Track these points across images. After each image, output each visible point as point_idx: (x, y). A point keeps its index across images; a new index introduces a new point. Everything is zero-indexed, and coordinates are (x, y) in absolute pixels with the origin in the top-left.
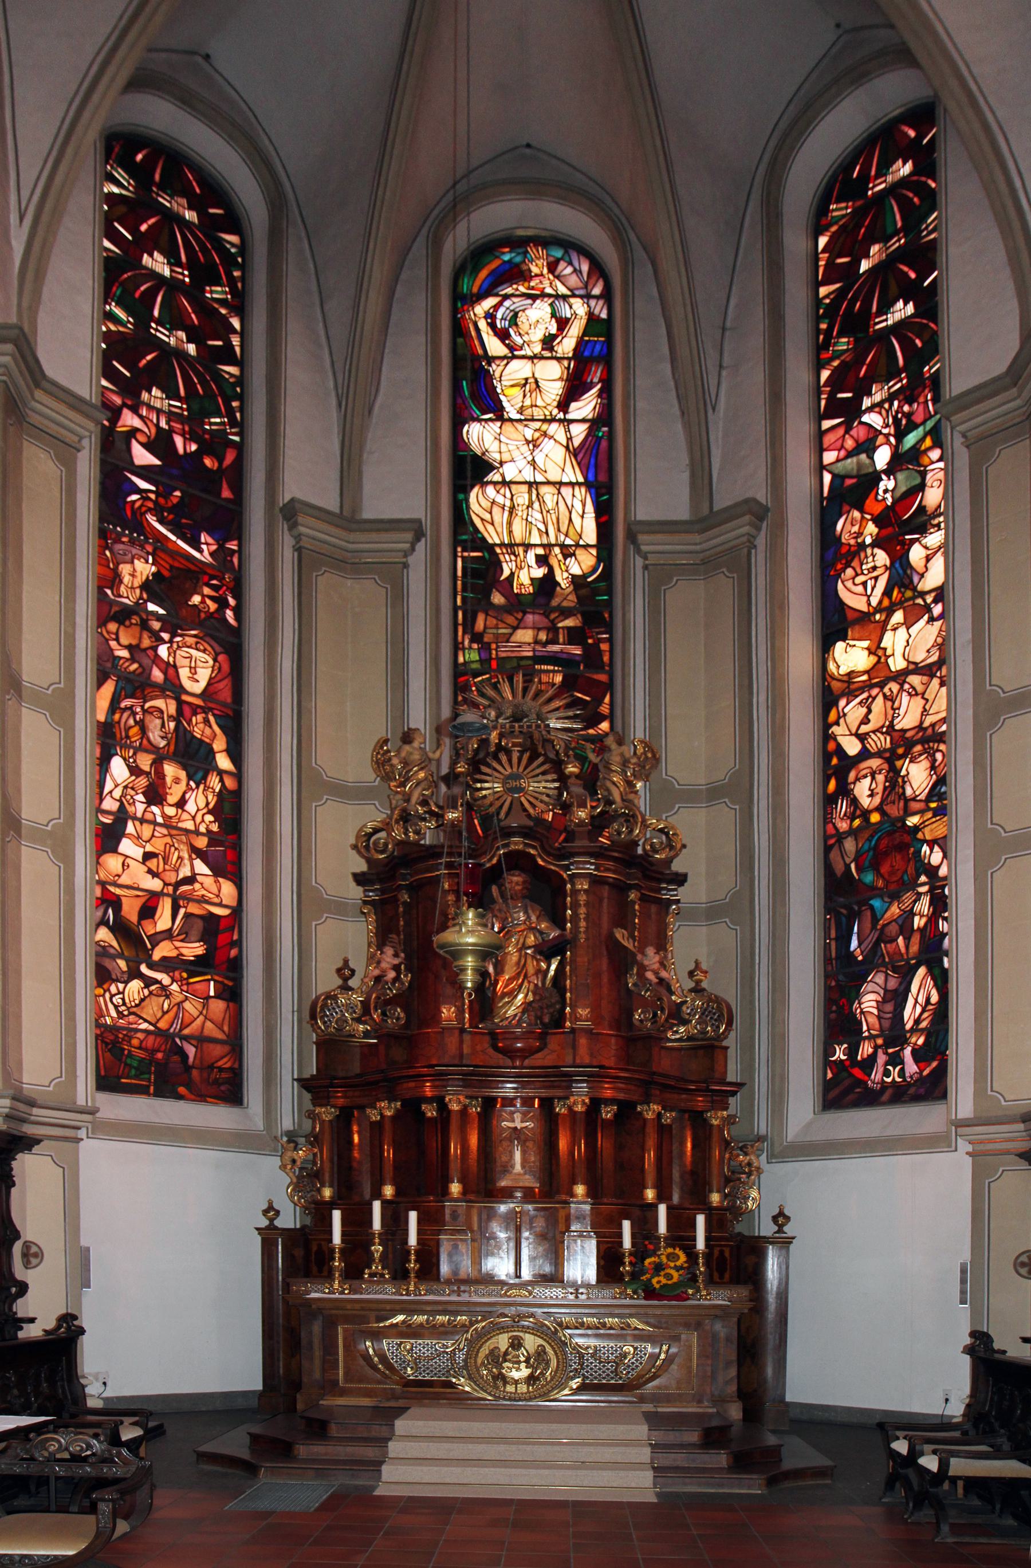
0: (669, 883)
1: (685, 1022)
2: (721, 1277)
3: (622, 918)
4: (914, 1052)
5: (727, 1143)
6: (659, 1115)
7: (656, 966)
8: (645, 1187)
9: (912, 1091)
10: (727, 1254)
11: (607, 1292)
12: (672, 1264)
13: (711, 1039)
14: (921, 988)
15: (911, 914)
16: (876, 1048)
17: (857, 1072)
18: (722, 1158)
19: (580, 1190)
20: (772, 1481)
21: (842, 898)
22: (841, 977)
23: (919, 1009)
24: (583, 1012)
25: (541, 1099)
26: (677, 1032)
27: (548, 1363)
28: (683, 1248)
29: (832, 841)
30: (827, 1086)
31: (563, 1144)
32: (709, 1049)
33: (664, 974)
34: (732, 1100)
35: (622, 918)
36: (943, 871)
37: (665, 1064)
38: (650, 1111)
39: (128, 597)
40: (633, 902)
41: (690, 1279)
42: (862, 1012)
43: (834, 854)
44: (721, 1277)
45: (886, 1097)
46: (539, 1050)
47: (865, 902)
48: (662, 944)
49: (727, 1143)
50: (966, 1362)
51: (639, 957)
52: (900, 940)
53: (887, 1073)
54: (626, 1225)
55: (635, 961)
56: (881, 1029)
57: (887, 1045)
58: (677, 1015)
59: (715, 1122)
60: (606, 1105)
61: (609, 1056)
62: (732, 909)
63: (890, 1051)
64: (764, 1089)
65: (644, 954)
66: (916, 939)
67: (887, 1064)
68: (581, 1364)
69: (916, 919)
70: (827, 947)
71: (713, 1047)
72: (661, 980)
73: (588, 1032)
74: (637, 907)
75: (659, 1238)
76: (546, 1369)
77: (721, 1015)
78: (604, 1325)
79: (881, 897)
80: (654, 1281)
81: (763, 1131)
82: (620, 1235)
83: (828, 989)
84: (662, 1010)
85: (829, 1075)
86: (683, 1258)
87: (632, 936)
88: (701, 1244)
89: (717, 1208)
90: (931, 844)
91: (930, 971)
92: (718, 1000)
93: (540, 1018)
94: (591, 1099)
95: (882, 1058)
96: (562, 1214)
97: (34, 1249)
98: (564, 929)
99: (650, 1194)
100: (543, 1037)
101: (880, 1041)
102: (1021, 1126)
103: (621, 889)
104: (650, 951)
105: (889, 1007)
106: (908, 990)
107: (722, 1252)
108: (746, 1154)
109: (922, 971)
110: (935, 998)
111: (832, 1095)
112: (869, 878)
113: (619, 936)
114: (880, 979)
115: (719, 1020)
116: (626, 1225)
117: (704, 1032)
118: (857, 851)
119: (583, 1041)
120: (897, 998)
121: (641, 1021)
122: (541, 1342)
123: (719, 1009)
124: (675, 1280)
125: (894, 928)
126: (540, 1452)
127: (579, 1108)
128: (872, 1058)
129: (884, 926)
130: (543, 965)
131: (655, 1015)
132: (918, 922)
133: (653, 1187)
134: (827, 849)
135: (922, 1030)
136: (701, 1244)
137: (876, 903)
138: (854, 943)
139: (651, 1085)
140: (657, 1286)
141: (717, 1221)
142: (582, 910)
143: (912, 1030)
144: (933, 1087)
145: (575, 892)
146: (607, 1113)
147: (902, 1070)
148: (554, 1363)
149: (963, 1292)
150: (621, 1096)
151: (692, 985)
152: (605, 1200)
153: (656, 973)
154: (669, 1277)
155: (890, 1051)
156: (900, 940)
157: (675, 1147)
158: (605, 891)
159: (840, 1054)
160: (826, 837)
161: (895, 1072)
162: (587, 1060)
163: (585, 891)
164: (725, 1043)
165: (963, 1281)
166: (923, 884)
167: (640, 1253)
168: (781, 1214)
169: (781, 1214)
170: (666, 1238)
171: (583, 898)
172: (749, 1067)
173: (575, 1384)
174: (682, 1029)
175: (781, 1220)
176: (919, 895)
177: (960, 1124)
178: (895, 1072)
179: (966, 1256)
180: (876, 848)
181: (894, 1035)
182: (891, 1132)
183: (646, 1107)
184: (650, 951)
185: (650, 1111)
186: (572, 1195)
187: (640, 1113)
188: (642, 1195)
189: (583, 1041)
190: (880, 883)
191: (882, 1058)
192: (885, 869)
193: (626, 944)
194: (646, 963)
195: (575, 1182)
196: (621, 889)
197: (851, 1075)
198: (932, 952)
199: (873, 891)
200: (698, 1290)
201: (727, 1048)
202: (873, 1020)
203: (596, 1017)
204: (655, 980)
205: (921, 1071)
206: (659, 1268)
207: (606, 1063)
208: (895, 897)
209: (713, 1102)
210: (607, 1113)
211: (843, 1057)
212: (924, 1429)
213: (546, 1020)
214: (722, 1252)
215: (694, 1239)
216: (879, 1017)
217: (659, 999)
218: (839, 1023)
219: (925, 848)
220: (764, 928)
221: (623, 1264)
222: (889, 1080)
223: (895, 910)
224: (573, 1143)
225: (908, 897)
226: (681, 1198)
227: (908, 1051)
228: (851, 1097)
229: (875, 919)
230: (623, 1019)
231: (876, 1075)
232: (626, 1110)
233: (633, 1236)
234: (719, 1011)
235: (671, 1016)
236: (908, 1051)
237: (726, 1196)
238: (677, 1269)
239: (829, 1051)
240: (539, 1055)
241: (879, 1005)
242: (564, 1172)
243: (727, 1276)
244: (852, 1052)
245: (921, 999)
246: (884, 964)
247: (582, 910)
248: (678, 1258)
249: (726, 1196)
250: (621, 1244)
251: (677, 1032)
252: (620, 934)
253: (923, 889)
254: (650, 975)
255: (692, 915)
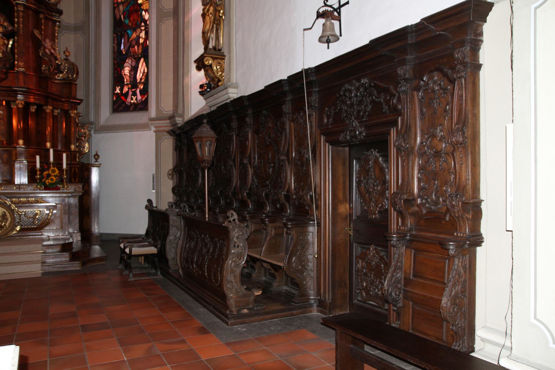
0: (56, 13)
1: (62, 72)
2: (75, 180)
3: (37, 26)
4: (140, 91)
5: (77, 124)
6: (52, 111)
7: (50, 47)
8: (46, 142)
9: (139, 106)
10: (77, 171)
11: (30, 188)
12: (53, 174)
13: (71, 80)
14: (142, 67)
15: (139, 37)
16: (129, 88)
17: (123, 98)
18: (75, 130)
19: (21, 142)
20: (83, 264)
21: (119, 29)
22: (118, 60)
23: (141, 75)
24: (21, 64)
25: (6, 102)
26: (59, 76)
27: (7, 220)
28: (58, 169)
29: (116, 5)
30: (114, 103)
31: (15, 122)
32: (70, 84)
33: (53, 51)
34: (78, 107)
35: (37, 26)
36: (148, 23)
37: (54, 89)
38: (49, 109)
39: (265, 231)
40: (41, 19)
41: (60, 181)
42: (125, 74)
43: (116, 11)
44: (75, 180)
45: (131, 109)
46: (5, 79)
47: (125, 31)
48: (53, 39)
49: (77, 124)
50: (146, 212)
51: (43, 43)
52: (136, 47)
53: (132, 99)
54: (38, 158)
55: (42, 45)
56: (130, 82)
57: (132, 88)
58: (58, 69)
59: (72, 115)
60: (32, 106)
61: (32, 85)
62: (81, 28)
63: (133, 90)
64: (93, 103)
65: (45, 42)
66: (140, 47)
67: (132, 95)
68: (20, 219)
69: (141, 39)
70: (114, 47)
71: (71, 83)
72: (52, 54)
73: (23, 73)
74: (43, 21)
75: (50, 163)
76: (6, 222)
77: (74, 70)
78: (29, 201)
79: (130, 29)
80: (47, 181)
81: (92, 120)
82: (35, 162)
83: (114, 64)
84: (52, 66)
85: (115, 99)
86: (57, 172)
87: (41, 34)
88: (65, 166)
89: (73, 151)
90: (146, 11)
91: (145, 61)
92: (73, 64)
93: (5, 65)
94: (25, 102)
95: (130, 93)
96: (14, 152)
97: (170, 177)
98: (14, 26)
99: (48, 145)
100: (6, 73)
101: (130, 86)
102: (168, 121)
103: (37, 13)
104: (47, 41)
105: (133, 73)
106: (138, 67)
107: (75, 170)
108: (84, 129)
109: (142, 60)
110: (146, 71)
111: (116, 106)
112: (127, 22)
113: (35, 33)
114: (130, 62)
115: (73, 72)
116: (38, 158)
117: (68, 77)
118: (124, 11)
119: (21, 77)
120: (134, 69)
121: (44, 70)
122: (5, 211)
123: (74, 68)
124: (54, 181)
125: (134, 42)
126: (25, 258)
127: (20, 106)
128: (128, 92)
129: (131, 41)
130: (6, 41)
131: (49, 68)
132: (141, 41)
133: (50, 142)
134: (114, 8)
135: (142, 83)
136: (65, 166)
137: (129, 32)
138: (122, 47)
139: (49, 98)
140: (48, 184)
141: (72, 157)
142: (21, 20)
143: (140, 83)
144: (143, 106)
145: (18, 11)
146: (33, 109)
147: (136, 98)
148: (9, 220)
149: (153, 186)
150: (37, 102)
151: (65, 57)
152: (32, 147)
153: (50, 50)
154: (52, 180)
155: (133, 90)
156: (136, 47)
157: (59, 125)
158: (31, 13)
159: (118, 91)
160: (114, 4)
161: (134, 98)
162: (23, 85)
163: (22, 11)
164: (76, 83)
165: (153, 182)
166: (143, 26)
167: (42, 170)
168: (97, 154)
169: (97, 154)
170: (53, 164)
171: (21, 14)
172: (87, 95)
173: (18, 228)
174: (61, 75)
175: (96, 157)
176: (142, 30)
177: (152, 120)
178: (134, 98)
179: (154, 172)
180: (129, 10)
181: (134, 84)
182: (133, 122)
183: (46, 107)
184: (47, 41)
185: (49, 109)
186: (18, 144)
187: (45, 110)
188: (45, 146)
189: (21, 77)
190: (130, 24)
191: (130, 93)
192: (132, 19)
193: (38, 36)
194: (46, 45)
195: (19, 139)
196: (37, 13)
197: (121, 99)
198: (145, 54)
199: (128, 27)
200: (64, 187)
201: (76, 85)
202: (128, 78)
203: (27, 67)
204: (49, 53)
205: (142, 98)
206: (49, 175)
207: (31, 87)
208: (134, 30)
209: (71, 106)
210: (33, 109)
211: (119, 92)
212: (133, 239)
213: (8, 66)
214: (75, 170)
215: (62, 164)
216: (130, 77)
217: (51, 62)
218: (118, 79)
219: (144, 13)
220: (93, 37)
221: (37, 175)
222: (132, 102)
223: (134, 35)
224: (19, 122)
225: (138, 30)
226: (62, 147)
227: (138, 91)
228: (121, 108)
229: (129, 38)
230: (38, 69)
231: (129, 100)
232: (40, 108)
233: (41, 162)
234: (73, 68)
235: (55, 69)
236: (138, 91)
237: (77, 146)
238: (55, 176)
239: (115, 89)
240: (5, 82)
241: (130, 71)
242: (15, 134)
243: (77, 180)
244: (121, 90)
245: (142, 71)
246: (131, 56)
247: (21, 20)
248: (55, 171)
249: (77, 146)
250: (36, 166)
251: (59, 76)
252: (36, 32)
253: (143, 28)
254: (47, 51)
255: (68, 28)
